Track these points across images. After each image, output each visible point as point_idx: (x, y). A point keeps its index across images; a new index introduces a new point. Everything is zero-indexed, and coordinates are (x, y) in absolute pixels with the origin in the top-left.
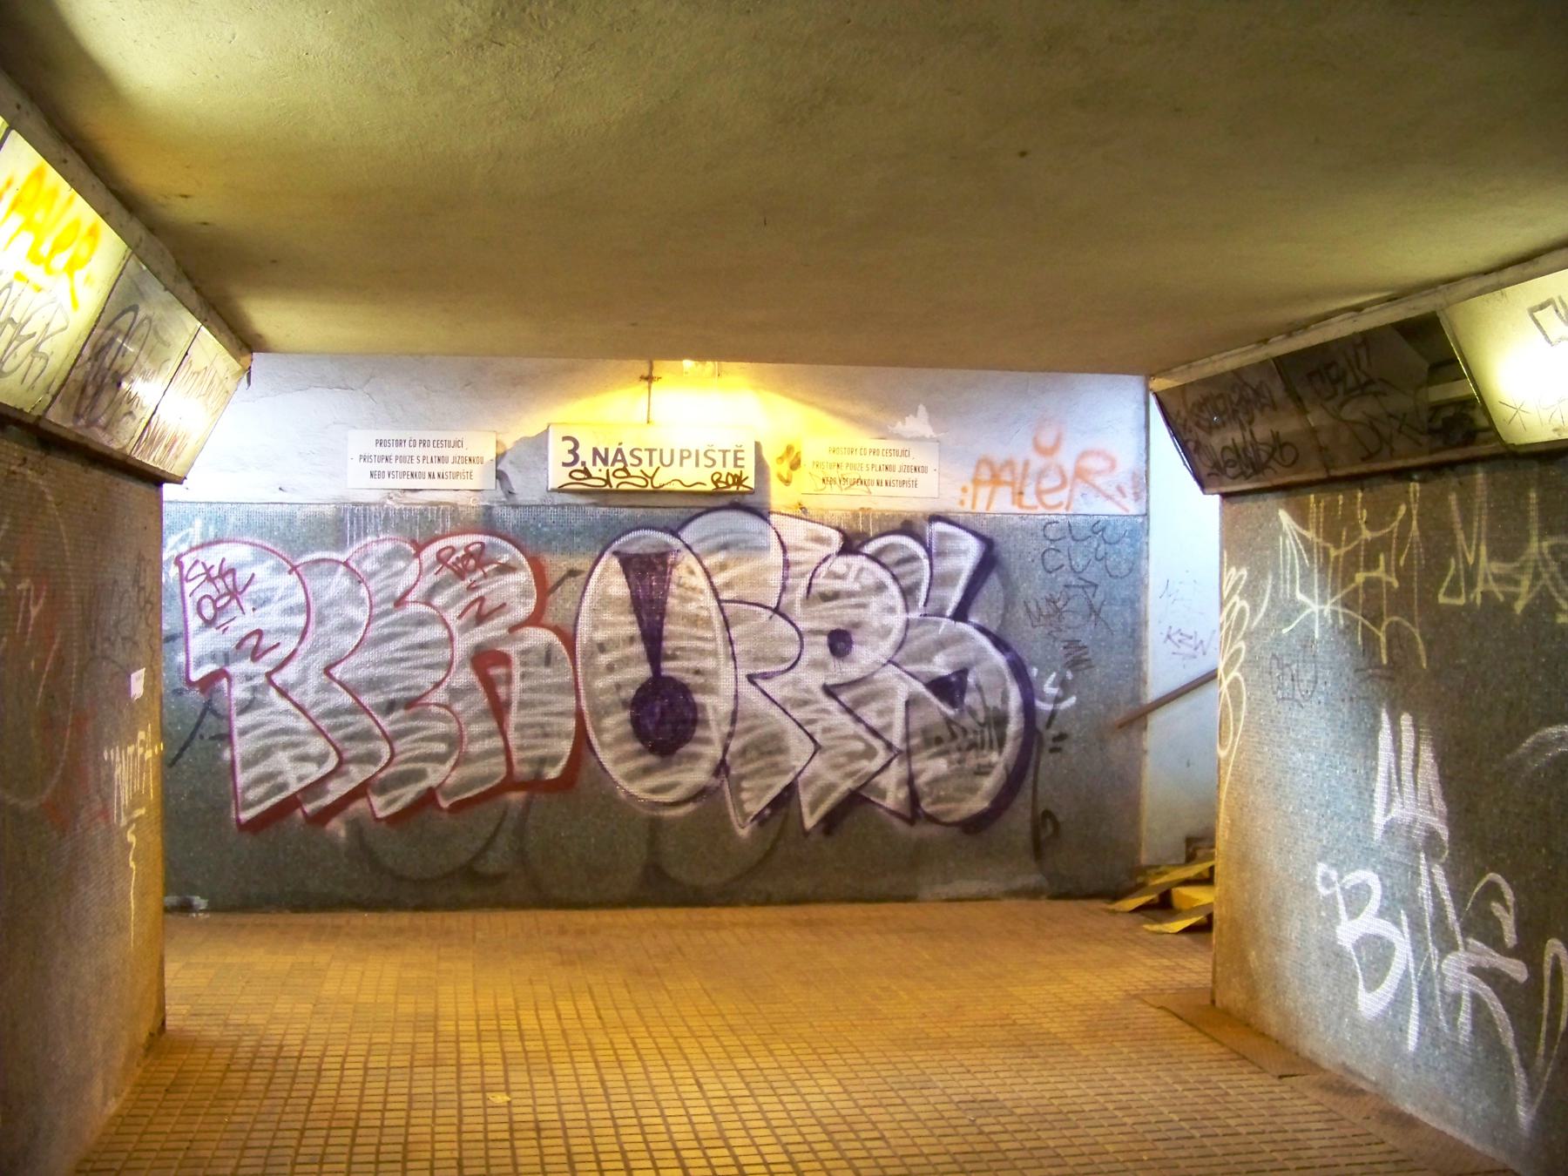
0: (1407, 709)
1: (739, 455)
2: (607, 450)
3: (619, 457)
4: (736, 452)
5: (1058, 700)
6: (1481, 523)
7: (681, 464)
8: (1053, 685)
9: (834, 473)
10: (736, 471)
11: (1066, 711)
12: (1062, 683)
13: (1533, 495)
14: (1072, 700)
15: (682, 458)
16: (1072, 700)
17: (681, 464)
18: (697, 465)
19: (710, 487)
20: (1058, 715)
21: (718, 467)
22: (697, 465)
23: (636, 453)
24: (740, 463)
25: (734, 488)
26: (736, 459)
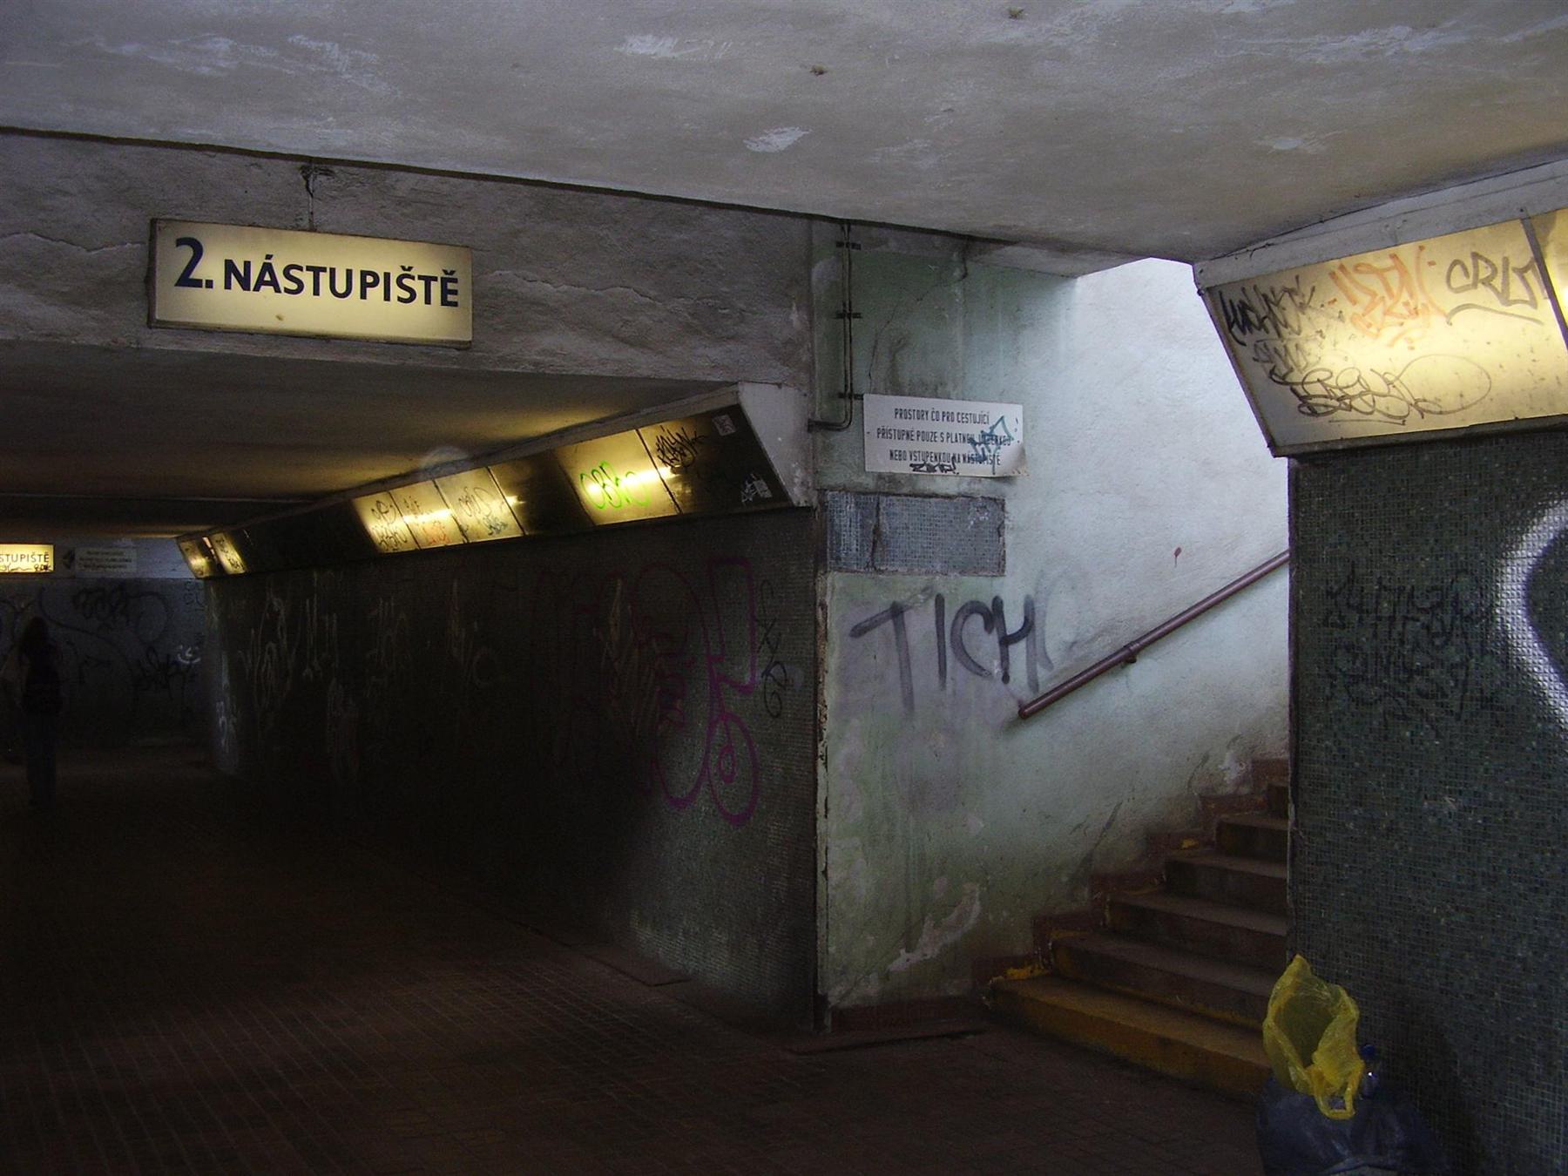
0: (1291, 554)
1: (450, 286)
2: (247, 265)
3: (267, 278)
4: (444, 282)
5: (191, 659)
6: (975, 408)
7: (363, 296)
8: (190, 653)
9: (89, 562)
10: (45, 564)
11: (196, 665)
12: (193, 652)
13: (212, 589)
14: (198, 660)
15: (364, 286)
16: (198, 660)
17: (363, 296)
18: (387, 298)
19: (34, 570)
20: (193, 667)
21: (37, 562)
22: (387, 298)
23: (293, 272)
24: (450, 298)
25: (44, 571)
26: (45, 558)
